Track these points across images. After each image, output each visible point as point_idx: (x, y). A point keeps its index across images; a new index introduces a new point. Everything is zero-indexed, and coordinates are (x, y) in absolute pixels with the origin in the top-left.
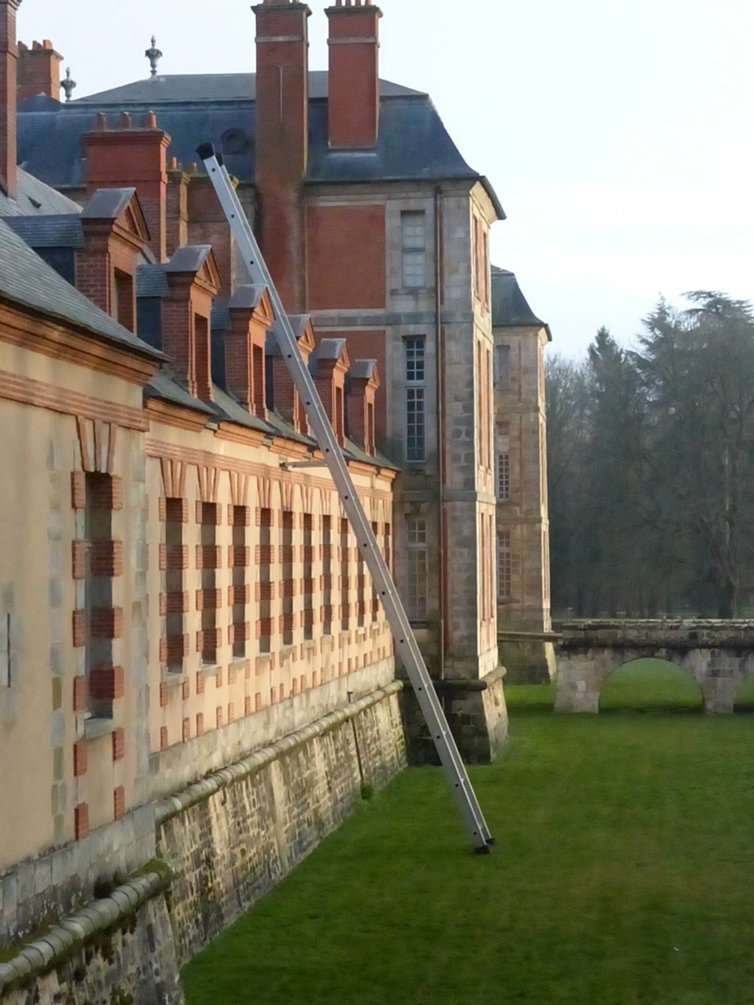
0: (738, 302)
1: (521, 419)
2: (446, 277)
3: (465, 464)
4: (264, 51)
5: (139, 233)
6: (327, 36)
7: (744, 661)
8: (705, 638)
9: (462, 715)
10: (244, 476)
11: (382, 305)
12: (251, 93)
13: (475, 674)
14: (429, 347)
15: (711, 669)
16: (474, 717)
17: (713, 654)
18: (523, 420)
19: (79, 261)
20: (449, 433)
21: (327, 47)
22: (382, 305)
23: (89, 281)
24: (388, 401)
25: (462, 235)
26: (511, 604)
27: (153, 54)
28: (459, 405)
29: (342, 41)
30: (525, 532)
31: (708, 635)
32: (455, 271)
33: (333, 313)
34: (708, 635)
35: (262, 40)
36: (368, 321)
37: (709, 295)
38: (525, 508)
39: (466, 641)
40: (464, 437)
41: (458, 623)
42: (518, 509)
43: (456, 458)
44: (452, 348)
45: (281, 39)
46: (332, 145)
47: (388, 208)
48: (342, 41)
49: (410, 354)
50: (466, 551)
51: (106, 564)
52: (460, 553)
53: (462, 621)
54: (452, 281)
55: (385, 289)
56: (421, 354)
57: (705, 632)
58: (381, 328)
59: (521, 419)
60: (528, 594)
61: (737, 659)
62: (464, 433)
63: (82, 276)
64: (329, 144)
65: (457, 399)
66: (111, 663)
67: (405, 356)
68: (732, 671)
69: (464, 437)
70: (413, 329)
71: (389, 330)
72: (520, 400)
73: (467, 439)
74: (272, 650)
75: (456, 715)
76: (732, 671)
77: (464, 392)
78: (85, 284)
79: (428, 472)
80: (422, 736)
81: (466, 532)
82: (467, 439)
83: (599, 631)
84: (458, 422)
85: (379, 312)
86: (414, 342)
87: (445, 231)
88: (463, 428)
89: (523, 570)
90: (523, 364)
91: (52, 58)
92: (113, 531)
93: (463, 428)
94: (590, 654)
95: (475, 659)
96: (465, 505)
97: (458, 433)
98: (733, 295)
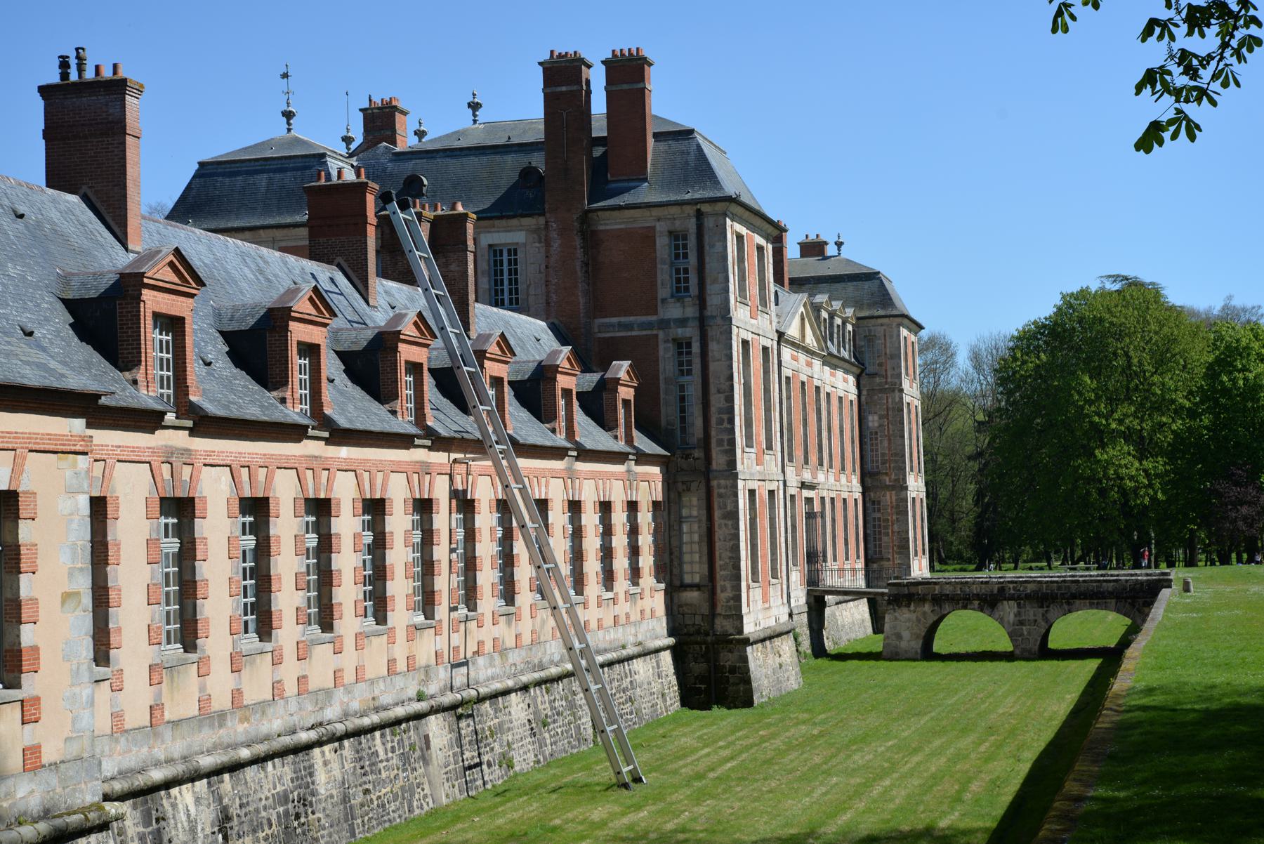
0: (1151, 283)
1: (887, 399)
2: (708, 287)
3: (728, 448)
4: (551, 101)
5: (191, 281)
6: (604, 84)
7: (1046, 611)
8: (1012, 592)
9: (730, 666)
10: (366, 475)
11: (655, 313)
12: (538, 134)
13: (741, 631)
14: (696, 348)
15: (1018, 618)
16: (739, 667)
17: (1019, 605)
18: (890, 400)
19: (120, 308)
20: (713, 421)
21: (604, 93)
22: (655, 313)
23: (128, 324)
24: (662, 396)
25: (721, 249)
26: (882, 563)
27: (474, 107)
28: (722, 396)
29: (614, 88)
30: (894, 498)
31: (1014, 588)
32: (715, 281)
33: (614, 320)
34: (1014, 588)
35: (549, 90)
36: (642, 326)
37: (1126, 278)
38: (893, 477)
39: (732, 602)
40: (726, 425)
41: (724, 586)
42: (887, 479)
43: (720, 442)
44: (713, 347)
45: (564, 89)
46: (612, 177)
47: (658, 228)
48: (614, 88)
49: (680, 354)
50: (730, 523)
51: (16, 563)
52: (726, 525)
53: (728, 585)
54: (712, 289)
55: (656, 298)
56: (689, 353)
57: (1011, 586)
58: (655, 332)
59: (887, 399)
60: (899, 553)
61: (1040, 610)
62: (726, 421)
63: (122, 320)
64: (609, 176)
65: (719, 392)
66: (20, 644)
67: (676, 356)
68: (1036, 621)
69: (726, 425)
70: (680, 332)
71: (661, 334)
72: (886, 383)
73: (729, 426)
74: (437, 617)
75: (724, 666)
76: (1036, 621)
77: (725, 386)
78: (125, 327)
79: (696, 455)
80: (695, 684)
81: (729, 508)
82: (729, 426)
83: (920, 587)
84: (720, 411)
85: (653, 318)
86: (682, 346)
87: (707, 247)
88: (725, 417)
89: (893, 532)
90: (888, 352)
91: (398, 115)
92: (20, 537)
93: (725, 417)
94: (912, 608)
95: (740, 617)
96: (729, 483)
97: (720, 422)
98: (1146, 278)
